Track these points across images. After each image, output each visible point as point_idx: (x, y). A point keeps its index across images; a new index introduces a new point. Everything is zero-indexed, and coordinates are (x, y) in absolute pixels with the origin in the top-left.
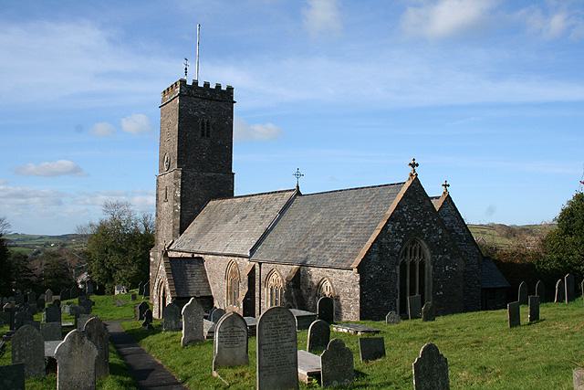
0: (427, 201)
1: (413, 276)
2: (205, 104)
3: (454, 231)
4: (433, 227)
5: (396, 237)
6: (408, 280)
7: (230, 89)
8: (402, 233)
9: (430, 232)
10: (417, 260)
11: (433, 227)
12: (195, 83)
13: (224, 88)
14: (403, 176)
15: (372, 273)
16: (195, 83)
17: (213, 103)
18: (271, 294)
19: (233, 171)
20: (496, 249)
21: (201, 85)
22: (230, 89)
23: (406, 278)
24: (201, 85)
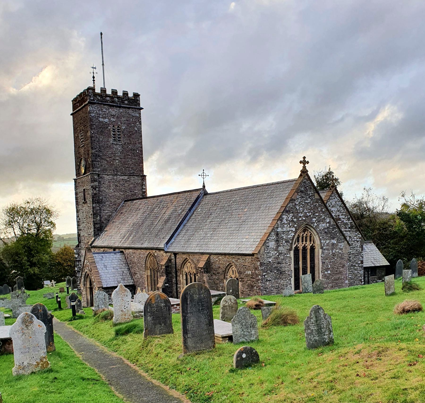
1: (305, 258)
2: (114, 111)
5: (290, 227)
6: (301, 263)
7: (136, 96)
10: (309, 245)
12: (103, 90)
13: (131, 95)
16: (103, 90)
22: (136, 96)
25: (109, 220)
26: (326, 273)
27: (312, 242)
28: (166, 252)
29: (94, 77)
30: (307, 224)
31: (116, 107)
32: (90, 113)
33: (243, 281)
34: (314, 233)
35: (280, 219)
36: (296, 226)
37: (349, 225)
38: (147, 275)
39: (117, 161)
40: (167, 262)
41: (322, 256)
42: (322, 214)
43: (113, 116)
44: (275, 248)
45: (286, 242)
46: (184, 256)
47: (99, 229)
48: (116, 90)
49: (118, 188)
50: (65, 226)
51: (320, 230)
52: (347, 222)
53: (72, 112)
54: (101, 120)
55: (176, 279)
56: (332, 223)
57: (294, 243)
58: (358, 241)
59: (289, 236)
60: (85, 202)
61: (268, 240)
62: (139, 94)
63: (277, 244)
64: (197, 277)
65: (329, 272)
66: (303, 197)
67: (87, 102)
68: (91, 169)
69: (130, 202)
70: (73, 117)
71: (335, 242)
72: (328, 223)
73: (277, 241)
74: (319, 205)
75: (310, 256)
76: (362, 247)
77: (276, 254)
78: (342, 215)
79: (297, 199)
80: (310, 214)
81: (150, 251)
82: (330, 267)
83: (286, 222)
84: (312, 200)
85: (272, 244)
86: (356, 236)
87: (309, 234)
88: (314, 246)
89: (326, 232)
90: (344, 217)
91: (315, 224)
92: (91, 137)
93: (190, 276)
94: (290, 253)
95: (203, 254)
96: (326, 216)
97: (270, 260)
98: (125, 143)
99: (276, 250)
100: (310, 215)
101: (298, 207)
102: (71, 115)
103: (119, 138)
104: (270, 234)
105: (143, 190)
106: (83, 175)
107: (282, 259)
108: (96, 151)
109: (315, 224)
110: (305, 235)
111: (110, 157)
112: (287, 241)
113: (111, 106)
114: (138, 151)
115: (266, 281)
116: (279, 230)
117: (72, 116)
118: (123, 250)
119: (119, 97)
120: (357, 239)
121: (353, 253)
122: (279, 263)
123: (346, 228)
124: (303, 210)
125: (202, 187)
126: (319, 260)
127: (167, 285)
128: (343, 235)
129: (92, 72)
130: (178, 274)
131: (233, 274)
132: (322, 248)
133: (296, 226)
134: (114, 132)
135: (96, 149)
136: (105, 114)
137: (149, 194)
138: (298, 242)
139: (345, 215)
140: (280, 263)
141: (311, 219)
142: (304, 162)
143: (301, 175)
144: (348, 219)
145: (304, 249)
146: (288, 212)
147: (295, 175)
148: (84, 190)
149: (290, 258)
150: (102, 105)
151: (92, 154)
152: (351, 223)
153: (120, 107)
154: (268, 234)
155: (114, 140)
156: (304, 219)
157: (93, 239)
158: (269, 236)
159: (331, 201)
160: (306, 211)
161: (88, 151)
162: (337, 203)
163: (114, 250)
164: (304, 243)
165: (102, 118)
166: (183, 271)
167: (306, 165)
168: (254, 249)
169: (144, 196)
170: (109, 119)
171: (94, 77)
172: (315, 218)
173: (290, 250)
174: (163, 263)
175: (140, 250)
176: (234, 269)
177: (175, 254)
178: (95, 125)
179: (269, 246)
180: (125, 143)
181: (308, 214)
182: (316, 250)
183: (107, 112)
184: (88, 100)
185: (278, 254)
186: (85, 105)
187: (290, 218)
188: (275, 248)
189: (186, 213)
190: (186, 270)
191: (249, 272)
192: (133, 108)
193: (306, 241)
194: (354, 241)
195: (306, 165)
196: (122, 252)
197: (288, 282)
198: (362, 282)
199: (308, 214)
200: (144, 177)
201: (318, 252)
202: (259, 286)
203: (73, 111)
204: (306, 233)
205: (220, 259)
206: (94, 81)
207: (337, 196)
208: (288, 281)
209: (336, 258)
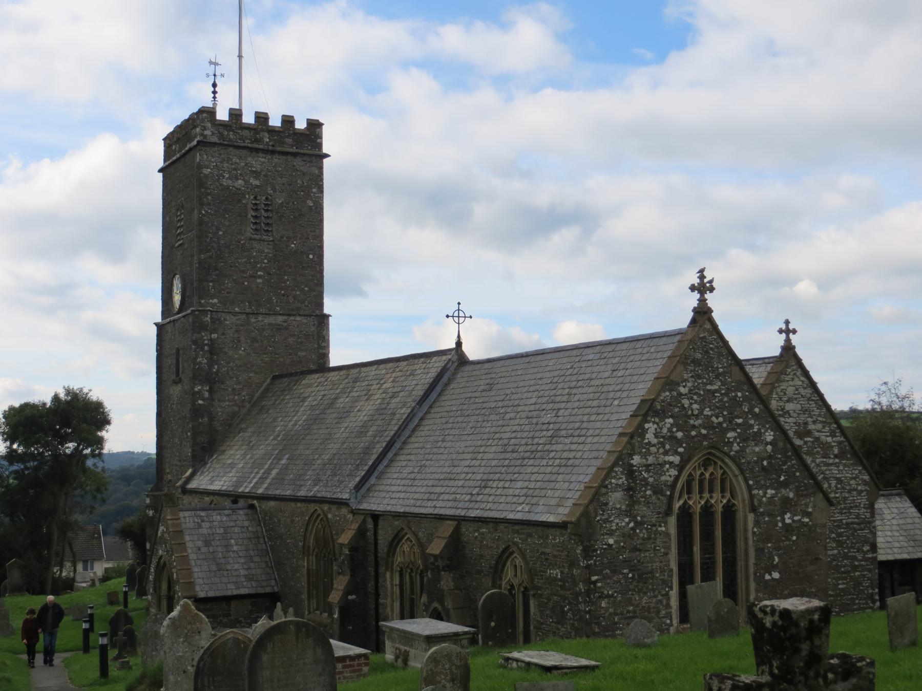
0: (736, 370)
1: (708, 536)
2: (258, 162)
3: (809, 433)
4: (752, 426)
5: (666, 453)
6: (697, 549)
7: (315, 126)
8: (679, 442)
9: (744, 439)
10: (718, 501)
11: (752, 426)
12: (236, 114)
13: (301, 125)
14: (677, 316)
15: (611, 533)
16: (236, 114)
17: (276, 159)
18: (401, 586)
19: (326, 311)
20: (575, 635)
21: (248, 118)
22: (315, 126)
23: (691, 545)
24: (248, 118)
25: (230, 425)
26: (767, 577)
27: (728, 495)
28: (354, 512)
29: (214, 85)
30: (712, 447)
31: (265, 151)
32: (200, 167)
33: (541, 595)
34: (730, 468)
35: (640, 431)
36: (681, 450)
37: (836, 451)
38: (308, 570)
39: (259, 281)
40: (355, 536)
41: (754, 533)
42: (752, 422)
43: (256, 174)
44: (624, 507)
45: (655, 493)
46: (397, 523)
47: (205, 449)
48: (266, 114)
49: (257, 345)
50: (132, 431)
51: (749, 463)
52: (829, 439)
53: (161, 164)
54: (225, 182)
55: (377, 581)
56: (781, 444)
57: (677, 495)
58: (862, 491)
59: (663, 478)
60: (176, 382)
61: (606, 487)
62: (321, 121)
63: (631, 497)
64: (425, 579)
65: (776, 575)
66: (699, 377)
67: (195, 143)
68: (195, 299)
69: (375, 367)
70: (164, 177)
71: (791, 495)
72: (771, 443)
73: (629, 490)
74: (744, 396)
75: (724, 530)
76: (871, 506)
77: (628, 524)
78: (814, 422)
79: (685, 381)
80: (721, 419)
81: (316, 506)
82: (777, 559)
83: (655, 441)
84: (724, 383)
85: (616, 498)
86: (855, 478)
87: (720, 472)
88: (734, 505)
89: (764, 469)
90: (819, 426)
91: (736, 447)
92: (201, 222)
93: (411, 577)
94: (666, 523)
95: (441, 518)
96: (764, 426)
97: (611, 541)
98: (282, 237)
99: (629, 513)
100: (720, 424)
101: (686, 402)
102: (160, 171)
103: (267, 224)
104: (611, 470)
105: (320, 351)
106: (178, 313)
107: (643, 539)
108: (211, 257)
109: (736, 447)
110: (707, 475)
111: (243, 272)
112: (657, 491)
113: (251, 150)
114: (311, 256)
115: (600, 597)
116: (636, 460)
117: (161, 174)
118: (255, 502)
119: (272, 131)
120: (858, 485)
121: (847, 524)
122: (635, 549)
123: (826, 456)
124: (701, 411)
125: (454, 346)
126: (746, 544)
127: (354, 597)
128: (812, 476)
129: (212, 73)
130: (382, 570)
131: (516, 575)
132: (754, 509)
133: (681, 450)
134: (256, 210)
135: (209, 251)
136: (235, 169)
137: (335, 360)
138: (689, 492)
139: (821, 422)
140: (640, 550)
141: (725, 431)
142: (703, 287)
143: (693, 321)
144: (833, 434)
145: (707, 511)
146: (661, 414)
147: (681, 319)
148: (178, 350)
149: (667, 535)
150: (231, 149)
151: (199, 263)
152: (840, 443)
153: (273, 152)
154: (605, 472)
155: (256, 230)
156: (704, 432)
157: (190, 471)
158: (608, 476)
159: (783, 386)
160: (709, 413)
161: (192, 256)
162: (802, 391)
163: (235, 502)
164: (706, 495)
165: (229, 178)
166: (393, 563)
167: (708, 296)
168: (567, 511)
169: (321, 365)
170: (246, 182)
171: (214, 85)
172: (734, 430)
173: (668, 512)
174: (345, 538)
175: (293, 504)
176: (519, 561)
177: (376, 517)
178: (209, 194)
179: (607, 504)
180: (282, 237)
181: (714, 419)
182: (740, 515)
183: (243, 164)
184: (198, 138)
185: (632, 525)
186: (191, 149)
187: (665, 430)
188: (624, 507)
189: (409, 410)
190: (399, 559)
191: (556, 573)
192: (304, 154)
193: (711, 491)
194: (850, 491)
195: (708, 296)
196: (252, 507)
197: (660, 602)
198: (874, 602)
199: (714, 419)
200: (323, 320)
201: (748, 522)
202: (579, 611)
203: (165, 161)
204: (711, 469)
205: (483, 534)
206: (214, 92)
207: (799, 373)
208: (660, 597)
209: (794, 538)
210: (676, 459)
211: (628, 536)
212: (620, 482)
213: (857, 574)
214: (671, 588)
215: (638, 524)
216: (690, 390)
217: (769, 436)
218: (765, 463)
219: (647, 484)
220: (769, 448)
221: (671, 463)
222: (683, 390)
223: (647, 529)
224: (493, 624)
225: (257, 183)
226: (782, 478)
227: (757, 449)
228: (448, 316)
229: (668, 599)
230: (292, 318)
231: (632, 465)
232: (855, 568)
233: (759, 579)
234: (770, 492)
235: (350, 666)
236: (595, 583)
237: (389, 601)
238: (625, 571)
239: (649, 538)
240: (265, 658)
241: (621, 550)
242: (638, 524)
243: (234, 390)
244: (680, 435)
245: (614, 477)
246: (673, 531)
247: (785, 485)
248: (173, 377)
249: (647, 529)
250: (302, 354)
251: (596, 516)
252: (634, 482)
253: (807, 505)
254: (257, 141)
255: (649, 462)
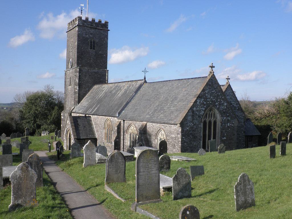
4: (222, 102)
5: (202, 107)
7: (106, 24)
8: (205, 105)
11: (222, 102)
15: (188, 127)
22: (106, 24)
27: (215, 118)
36: (205, 107)
42: (222, 101)
43: (91, 34)
45: (199, 117)
58: (242, 119)
65: (225, 138)
71: (230, 119)
72: (226, 106)
73: (193, 116)
80: (215, 100)
84: (216, 91)
85: (190, 118)
90: (234, 102)
94: (201, 124)
97: (188, 129)
100: (215, 101)
107: (195, 128)
110: (211, 113)
112: (199, 117)
116: (195, 109)
122: (193, 131)
123: (235, 110)
124: (210, 97)
133: (205, 107)
139: (235, 101)
140: (194, 131)
141: (215, 103)
145: (210, 122)
153: (96, 29)
156: (211, 102)
167: (213, 69)
170: (89, 36)
176: (163, 132)
179: (187, 119)
188: (191, 120)
190: (130, 131)
191: (174, 136)
197: (198, 144)
210: (204, 109)
211: (192, 128)
212: (191, 114)
213: (240, 138)
214: (201, 141)
215: (194, 125)
216: (208, 92)
217: (225, 104)
218: (224, 111)
219: (197, 115)
220: (225, 107)
221: (203, 110)
222: (206, 92)
223: (196, 126)
224: (162, 148)
225: (92, 36)
226: (228, 115)
227: (222, 107)
228: (142, 71)
229: (200, 143)
230: (99, 70)
231: (194, 110)
232: (240, 137)
233: (221, 139)
234: (225, 118)
235: (129, 158)
236: (183, 139)
237: (127, 141)
238: (191, 136)
239: (197, 128)
240: (141, 160)
241: (190, 131)
242: (194, 125)
243: (85, 88)
244: (205, 103)
245: (189, 113)
246: (202, 127)
247: (228, 116)
248: (69, 84)
249: (196, 126)
250: (101, 80)
251: (185, 122)
252: (194, 114)
253: (233, 122)
254: (92, 25)
255: (198, 109)
